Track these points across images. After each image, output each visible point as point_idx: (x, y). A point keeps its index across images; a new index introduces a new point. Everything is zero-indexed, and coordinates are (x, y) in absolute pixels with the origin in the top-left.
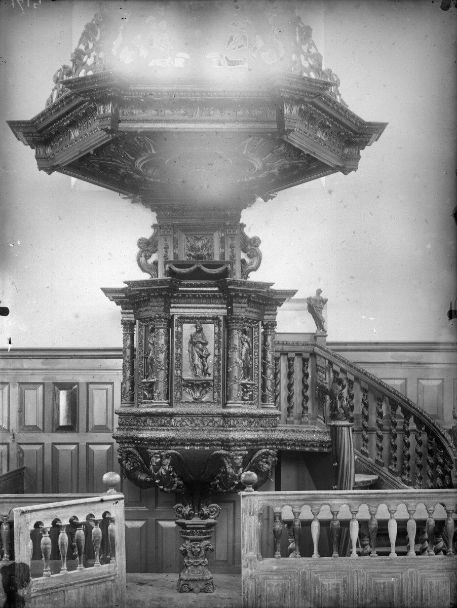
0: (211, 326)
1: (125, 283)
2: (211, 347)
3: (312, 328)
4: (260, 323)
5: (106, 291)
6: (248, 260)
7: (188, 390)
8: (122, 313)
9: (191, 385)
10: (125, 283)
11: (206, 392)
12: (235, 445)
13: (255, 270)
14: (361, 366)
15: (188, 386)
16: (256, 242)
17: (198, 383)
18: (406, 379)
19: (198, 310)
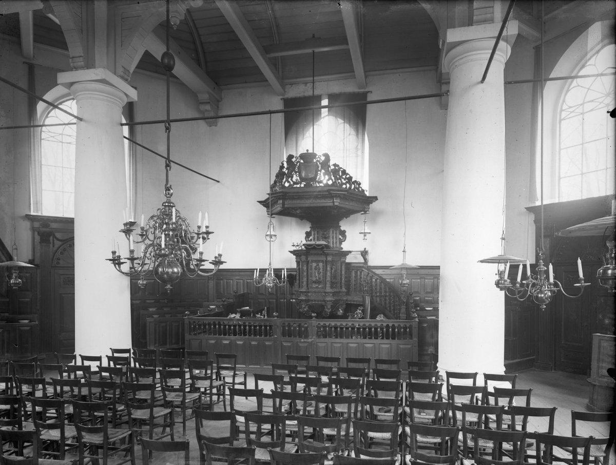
0: (321, 264)
2: (321, 270)
3: (363, 261)
5: (290, 252)
9: (315, 282)
16: (344, 232)
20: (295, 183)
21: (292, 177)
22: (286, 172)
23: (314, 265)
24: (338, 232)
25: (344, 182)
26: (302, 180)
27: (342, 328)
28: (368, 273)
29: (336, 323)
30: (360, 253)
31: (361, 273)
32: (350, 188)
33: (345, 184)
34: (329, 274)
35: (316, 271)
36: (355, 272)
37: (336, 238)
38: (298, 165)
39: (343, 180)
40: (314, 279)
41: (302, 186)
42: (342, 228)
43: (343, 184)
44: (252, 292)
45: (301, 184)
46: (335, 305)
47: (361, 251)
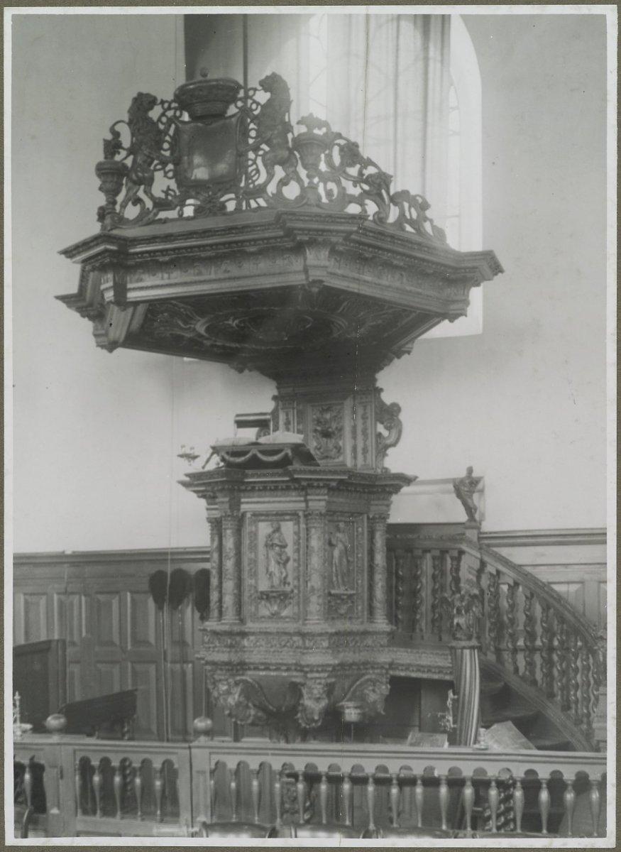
0: (290, 524)
1: (187, 475)
2: (290, 551)
4: (365, 516)
6: (385, 433)
7: (263, 602)
8: (207, 509)
9: (266, 597)
10: (187, 475)
11: (286, 607)
12: (312, 671)
13: (394, 445)
14: (529, 569)
15: (262, 599)
17: (274, 594)
18: (582, 582)
19: (273, 505)
20: (161, 205)
21: (149, 182)
22: (129, 162)
23: (264, 529)
24: (371, 412)
25: (355, 191)
26: (188, 187)
27: (335, 780)
28: (483, 564)
29: (243, 758)
30: (451, 487)
31: (457, 560)
32: (380, 218)
33: (359, 200)
34: (316, 561)
35: (272, 554)
36: (434, 558)
37: (364, 432)
38: (171, 132)
39: (345, 183)
40: (264, 586)
41: (189, 212)
42: (387, 398)
43: (346, 199)
44: (76, 638)
45: (183, 205)
46: (344, 677)
47: (454, 481)
